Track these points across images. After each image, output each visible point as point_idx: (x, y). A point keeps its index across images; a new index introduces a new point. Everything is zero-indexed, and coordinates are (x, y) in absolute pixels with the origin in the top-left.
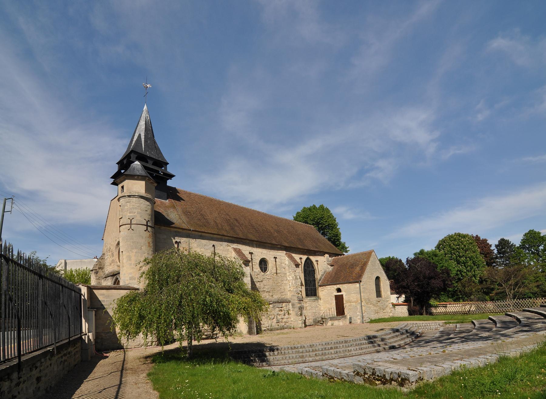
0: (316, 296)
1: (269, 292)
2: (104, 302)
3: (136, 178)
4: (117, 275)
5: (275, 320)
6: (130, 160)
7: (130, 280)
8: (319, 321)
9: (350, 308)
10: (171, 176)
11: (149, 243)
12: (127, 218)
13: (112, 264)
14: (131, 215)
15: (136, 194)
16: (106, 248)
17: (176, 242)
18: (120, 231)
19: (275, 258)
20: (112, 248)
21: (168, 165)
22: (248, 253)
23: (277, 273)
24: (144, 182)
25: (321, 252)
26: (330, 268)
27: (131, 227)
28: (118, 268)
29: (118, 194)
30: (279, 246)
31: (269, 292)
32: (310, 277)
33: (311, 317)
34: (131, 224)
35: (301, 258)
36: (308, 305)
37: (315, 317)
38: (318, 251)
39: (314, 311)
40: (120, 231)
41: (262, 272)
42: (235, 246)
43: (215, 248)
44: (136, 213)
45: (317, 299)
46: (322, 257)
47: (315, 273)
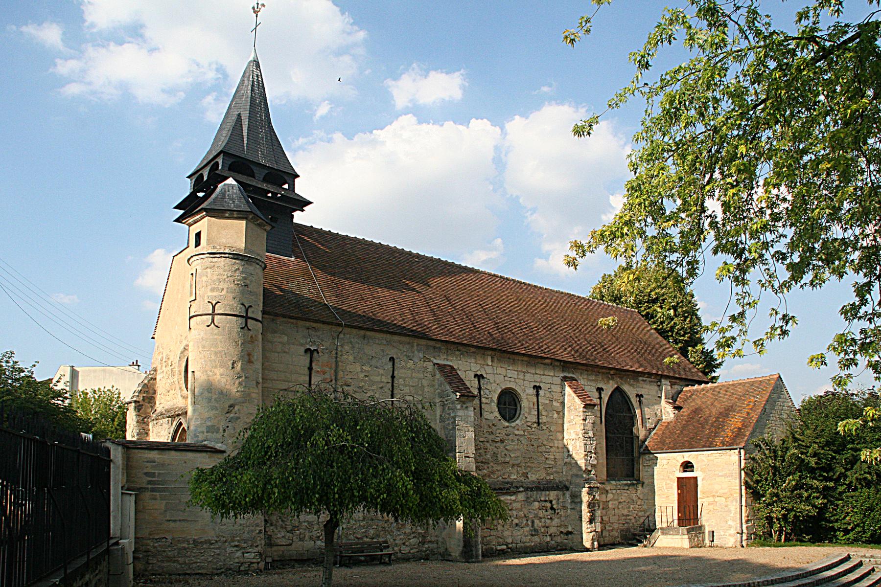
1: (518, 465)
2: (154, 477)
3: (227, 215)
4: (181, 417)
6: (216, 172)
7: (207, 432)
8: (635, 535)
9: (712, 509)
10: (303, 204)
12: (206, 301)
13: (172, 392)
14: (215, 294)
15: (227, 251)
16: (160, 358)
18: (190, 328)
19: (537, 388)
20: (171, 359)
21: (297, 180)
22: (473, 376)
23: (539, 423)
24: (244, 222)
27: (213, 321)
28: (184, 400)
29: (188, 243)
30: (547, 361)
31: (518, 465)
32: (620, 434)
35: (600, 390)
37: (626, 525)
39: (625, 512)
40: (190, 328)
41: (503, 421)
43: (396, 365)
44: (225, 289)
45: (633, 484)
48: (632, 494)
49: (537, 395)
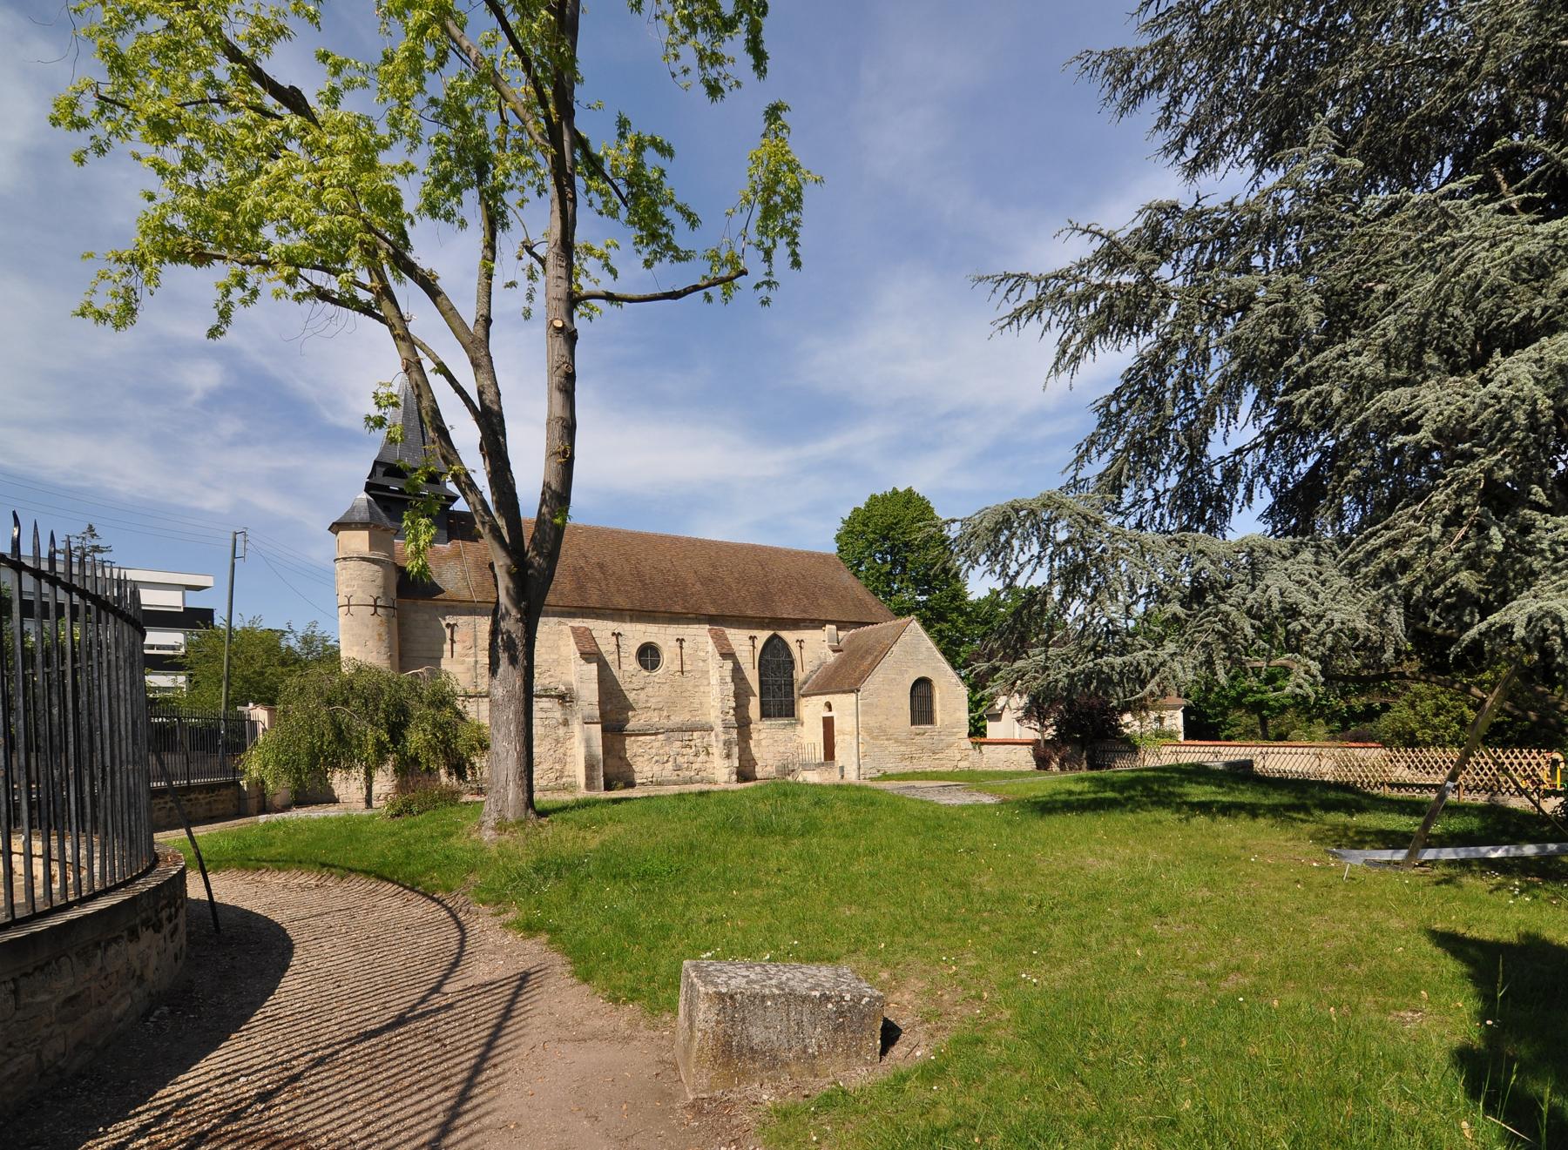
0: (793, 715)
1: (661, 709)
5: (670, 766)
11: (380, 635)
17: (448, 625)
19: (681, 641)
24: (366, 534)
25: (812, 621)
26: (832, 657)
31: (661, 709)
33: (770, 762)
34: (349, 605)
35: (753, 638)
36: (763, 735)
38: (804, 620)
39: (782, 749)
42: (578, 623)
46: (820, 631)
47: (793, 668)
48: (789, 732)
49: (681, 647)
